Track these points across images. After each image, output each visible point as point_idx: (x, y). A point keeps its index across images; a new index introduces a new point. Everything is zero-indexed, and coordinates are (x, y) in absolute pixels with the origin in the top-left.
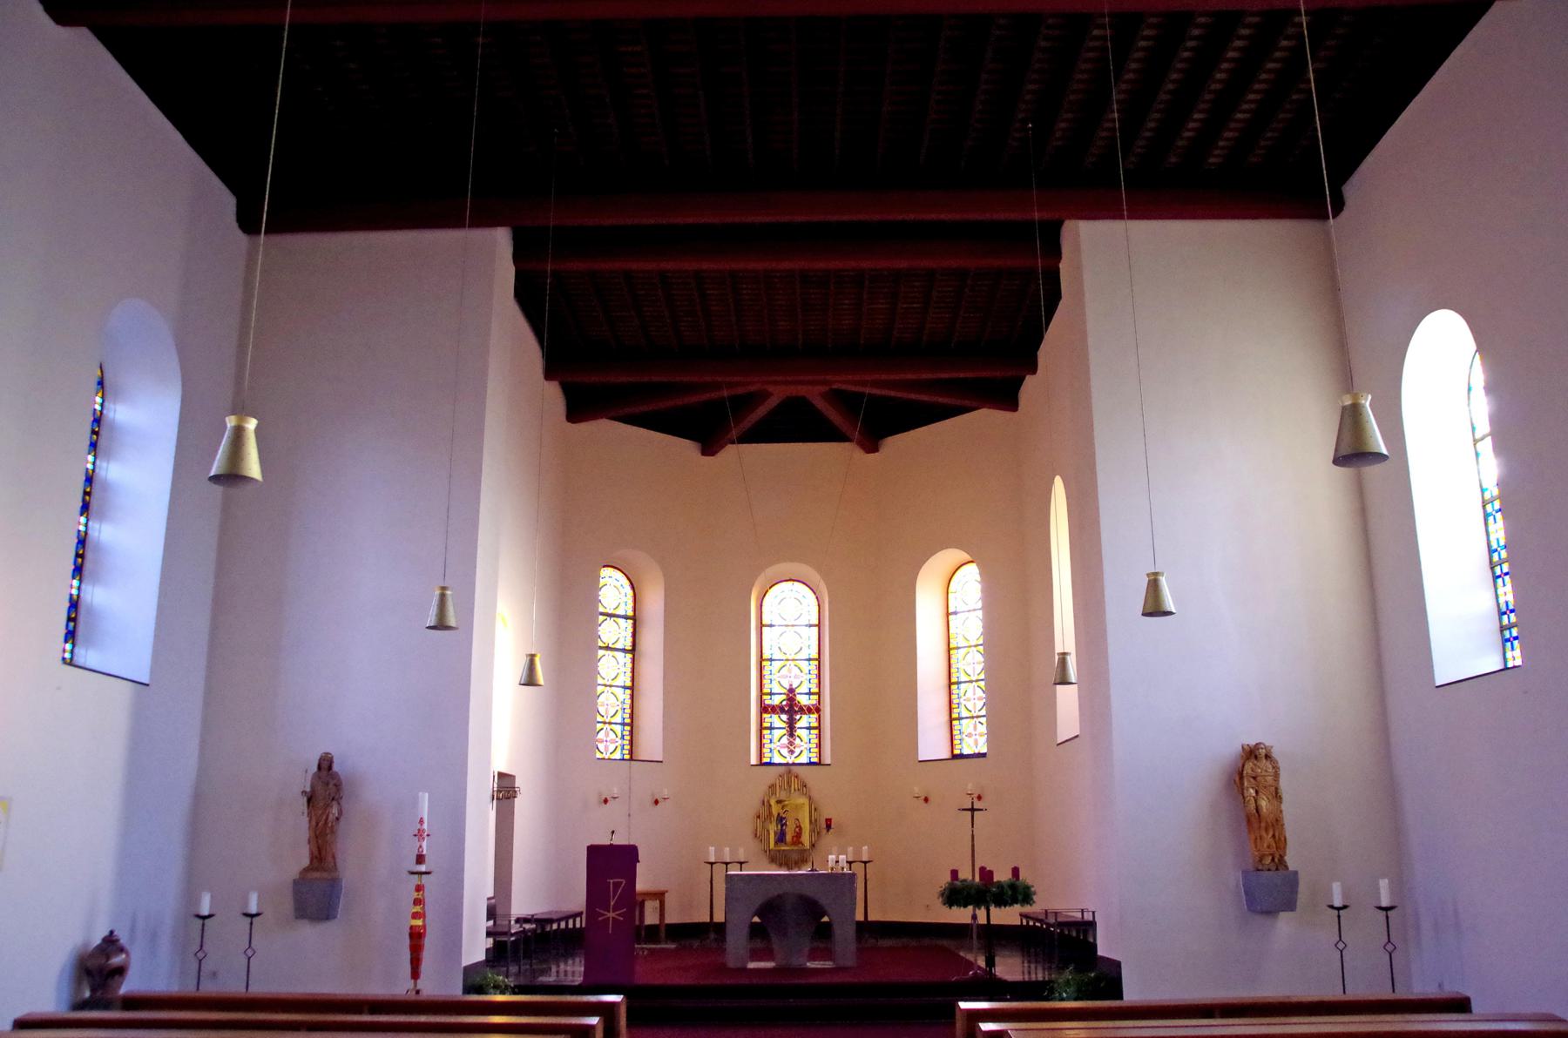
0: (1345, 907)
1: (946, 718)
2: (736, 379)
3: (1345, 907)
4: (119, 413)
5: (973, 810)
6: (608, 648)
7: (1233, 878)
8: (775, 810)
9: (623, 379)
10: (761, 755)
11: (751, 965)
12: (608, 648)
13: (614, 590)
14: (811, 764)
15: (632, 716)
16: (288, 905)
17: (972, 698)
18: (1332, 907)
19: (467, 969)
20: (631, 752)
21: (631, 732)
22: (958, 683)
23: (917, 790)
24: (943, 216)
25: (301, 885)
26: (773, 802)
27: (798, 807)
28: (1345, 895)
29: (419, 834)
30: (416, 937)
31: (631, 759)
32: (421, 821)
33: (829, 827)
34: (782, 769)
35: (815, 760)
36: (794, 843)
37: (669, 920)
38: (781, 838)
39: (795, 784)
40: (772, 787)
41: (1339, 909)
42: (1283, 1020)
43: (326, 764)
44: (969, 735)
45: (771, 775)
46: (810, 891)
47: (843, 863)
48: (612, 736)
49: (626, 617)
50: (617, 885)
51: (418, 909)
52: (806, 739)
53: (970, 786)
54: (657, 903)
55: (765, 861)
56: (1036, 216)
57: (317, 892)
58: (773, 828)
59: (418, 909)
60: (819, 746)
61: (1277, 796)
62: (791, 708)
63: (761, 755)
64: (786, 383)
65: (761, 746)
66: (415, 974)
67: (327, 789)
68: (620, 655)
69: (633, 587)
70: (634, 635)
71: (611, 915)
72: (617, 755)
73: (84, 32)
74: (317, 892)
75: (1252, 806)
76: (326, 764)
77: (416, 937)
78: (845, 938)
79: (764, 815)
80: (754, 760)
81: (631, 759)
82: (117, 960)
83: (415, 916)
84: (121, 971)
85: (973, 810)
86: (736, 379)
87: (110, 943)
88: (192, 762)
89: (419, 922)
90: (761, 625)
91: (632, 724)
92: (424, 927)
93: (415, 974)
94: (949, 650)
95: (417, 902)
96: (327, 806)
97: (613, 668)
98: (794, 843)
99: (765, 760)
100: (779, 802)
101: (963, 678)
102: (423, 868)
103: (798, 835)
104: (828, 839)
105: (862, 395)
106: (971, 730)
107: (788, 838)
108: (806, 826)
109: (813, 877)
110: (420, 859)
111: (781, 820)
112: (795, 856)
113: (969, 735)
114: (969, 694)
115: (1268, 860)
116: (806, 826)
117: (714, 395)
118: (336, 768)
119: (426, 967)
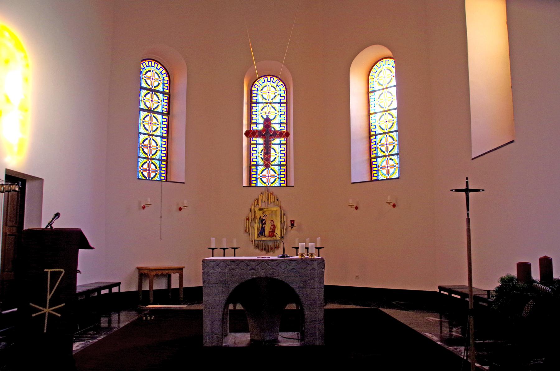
1: (366, 157)
5: (467, 191)
6: (149, 111)
8: (259, 214)
10: (250, 181)
12: (149, 111)
13: (153, 75)
17: (387, 144)
21: (166, 166)
22: (376, 135)
23: (351, 202)
26: (257, 209)
27: (273, 213)
30: (468, 220)
33: (292, 225)
34: (264, 189)
36: (269, 236)
37: (185, 285)
38: (262, 232)
39: (271, 198)
40: (256, 200)
44: (383, 168)
45: (256, 194)
46: (282, 275)
47: (312, 250)
50: (55, 276)
53: (389, 198)
54: (178, 275)
55: (252, 247)
58: (256, 226)
60: (286, 176)
62: (267, 133)
63: (250, 181)
65: (250, 176)
68: (159, 117)
69: (168, 75)
70: (169, 104)
71: (47, 310)
77: (468, 220)
78: (315, 315)
79: (251, 219)
80: (245, 183)
85: (467, 191)
90: (250, 103)
91: (167, 161)
94: (369, 114)
97: (151, 125)
98: (269, 236)
100: (260, 209)
101: (379, 131)
103: (273, 231)
104: (292, 232)
106: (384, 164)
107: (267, 233)
108: (278, 226)
109: (285, 262)
111: (262, 221)
112: (271, 244)
113: (383, 168)
114: (383, 141)
116: (278, 226)
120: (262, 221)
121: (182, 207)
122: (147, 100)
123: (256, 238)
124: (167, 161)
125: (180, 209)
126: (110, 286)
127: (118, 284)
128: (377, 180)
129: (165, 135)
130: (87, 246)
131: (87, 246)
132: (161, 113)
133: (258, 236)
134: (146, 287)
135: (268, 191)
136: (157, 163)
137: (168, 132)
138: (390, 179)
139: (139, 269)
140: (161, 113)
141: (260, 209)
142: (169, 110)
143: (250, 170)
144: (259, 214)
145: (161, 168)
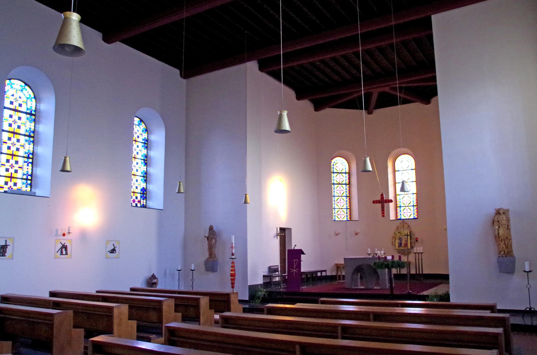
0: (530, 271)
2: (391, 83)
3: (530, 271)
4: (153, 138)
7: (494, 259)
9: (429, 76)
11: (376, 288)
13: (340, 164)
14: (415, 218)
15: (350, 206)
16: (203, 267)
18: (525, 271)
19: (249, 286)
20: (350, 218)
21: (350, 211)
24: (347, 35)
25: (206, 262)
28: (530, 265)
29: (232, 247)
30: (233, 275)
31: (350, 220)
32: (232, 244)
33: (417, 241)
35: (416, 217)
38: (400, 245)
39: (406, 226)
41: (528, 272)
42: (476, 311)
43: (211, 228)
48: (343, 213)
49: (346, 173)
51: (232, 269)
52: (412, 210)
56: (393, 23)
57: (211, 265)
58: (397, 241)
59: (232, 269)
61: (508, 228)
63: (397, 216)
64: (377, 87)
66: (233, 287)
67: (212, 235)
70: (349, 178)
71: (294, 271)
72: (345, 219)
73: (118, 43)
74: (211, 265)
75: (497, 232)
76: (211, 228)
77: (233, 275)
79: (394, 238)
81: (350, 220)
82: (155, 281)
83: (232, 270)
84: (155, 284)
86: (391, 83)
87: (153, 277)
88: (182, 229)
89: (232, 272)
90: (394, 171)
92: (235, 274)
93: (233, 287)
95: (232, 267)
96: (212, 240)
99: (398, 218)
100: (399, 232)
102: (233, 257)
105: (354, 98)
107: (403, 245)
110: (233, 254)
111: (400, 239)
115: (502, 253)
117: (352, 97)
118: (214, 229)
119: (236, 285)
120: (400, 239)
121: (66, 233)
122: (336, 178)
123: (397, 247)
124: (350, 209)
125: (357, 234)
126: (321, 271)
127: (325, 271)
128: (35, 111)
129: (348, 195)
130: (303, 253)
131: (303, 253)
132: (346, 184)
133: (399, 247)
134: (339, 274)
135: (403, 222)
136: (345, 210)
137: (349, 194)
138: (26, 84)
139: (336, 264)
140: (346, 184)
141: (399, 232)
142: (349, 182)
143: (396, 210)
144: (398, 235)
145: (347, 213)
